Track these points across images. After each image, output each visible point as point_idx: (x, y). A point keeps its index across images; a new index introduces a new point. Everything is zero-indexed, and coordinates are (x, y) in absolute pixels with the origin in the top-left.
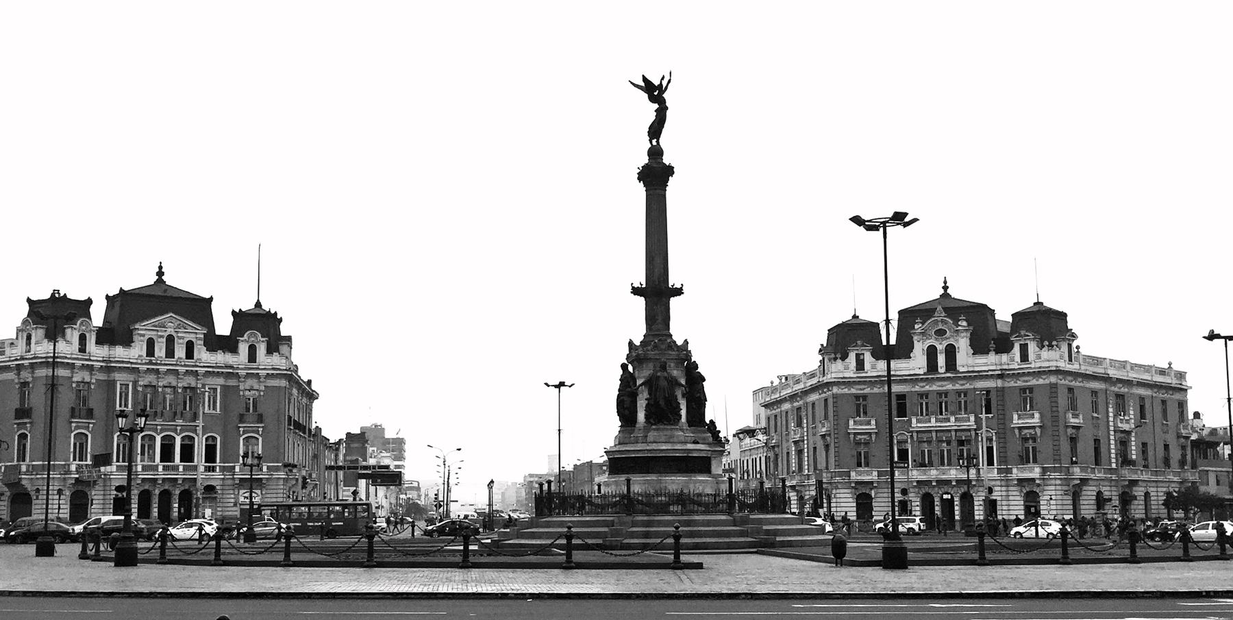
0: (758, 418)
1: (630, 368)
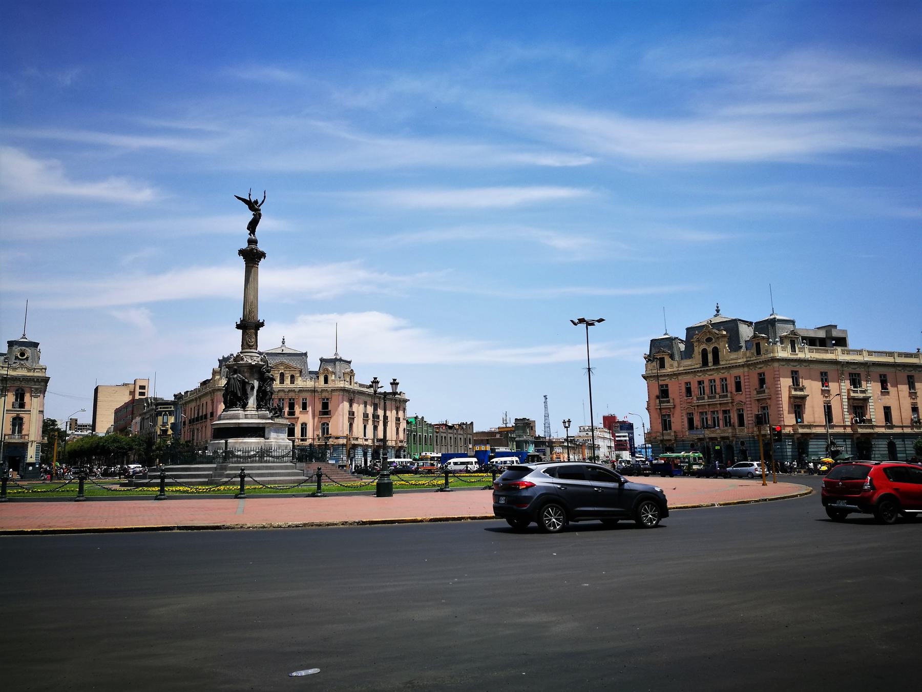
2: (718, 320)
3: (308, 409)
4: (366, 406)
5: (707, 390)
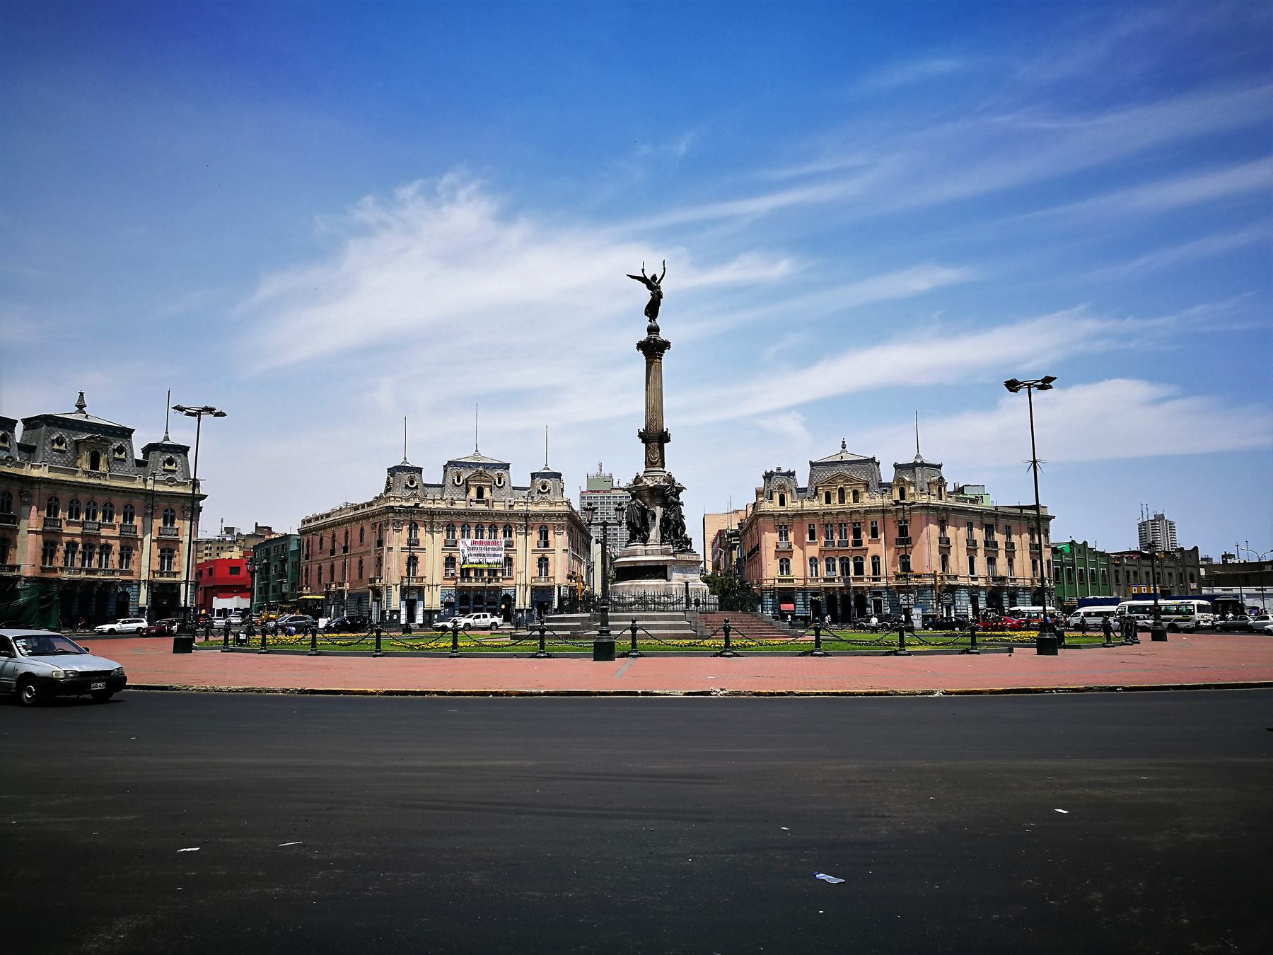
3: (879, 537)
4: (971, 530)
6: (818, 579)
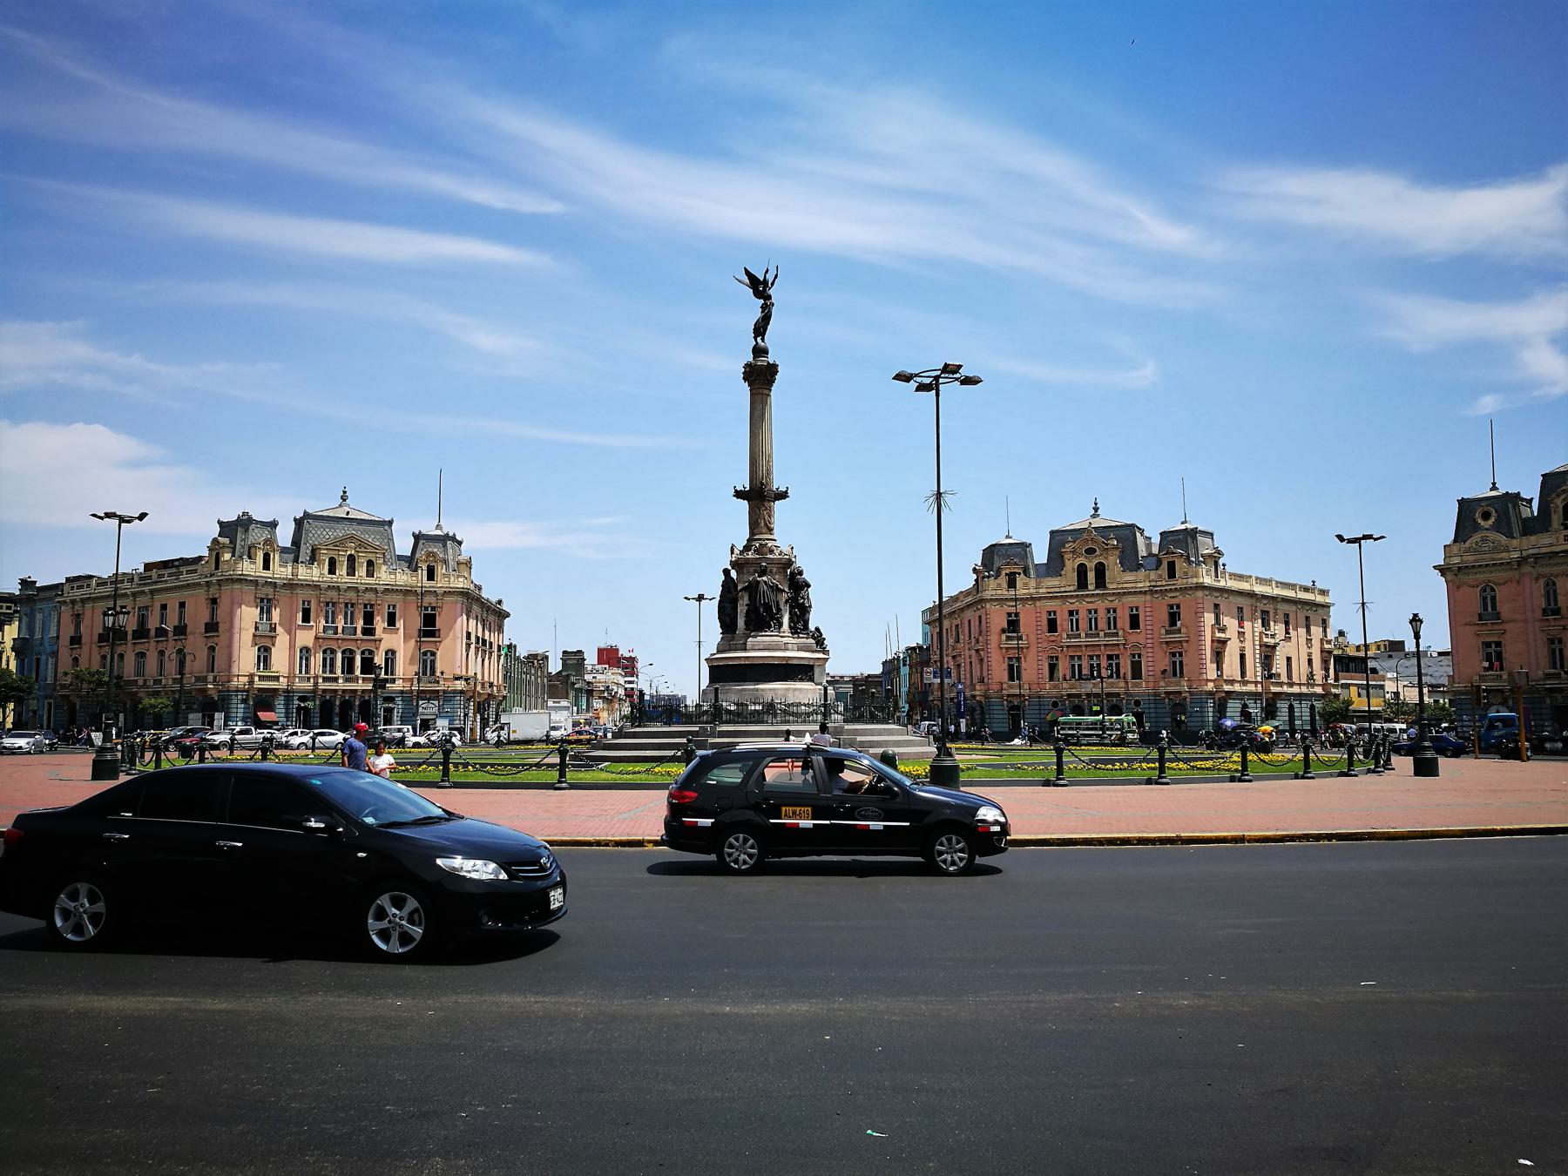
0: (925, 635)
1: (734, 574)
2: (1097, 523)
5: (1083, 625)
6: (309, 678)
